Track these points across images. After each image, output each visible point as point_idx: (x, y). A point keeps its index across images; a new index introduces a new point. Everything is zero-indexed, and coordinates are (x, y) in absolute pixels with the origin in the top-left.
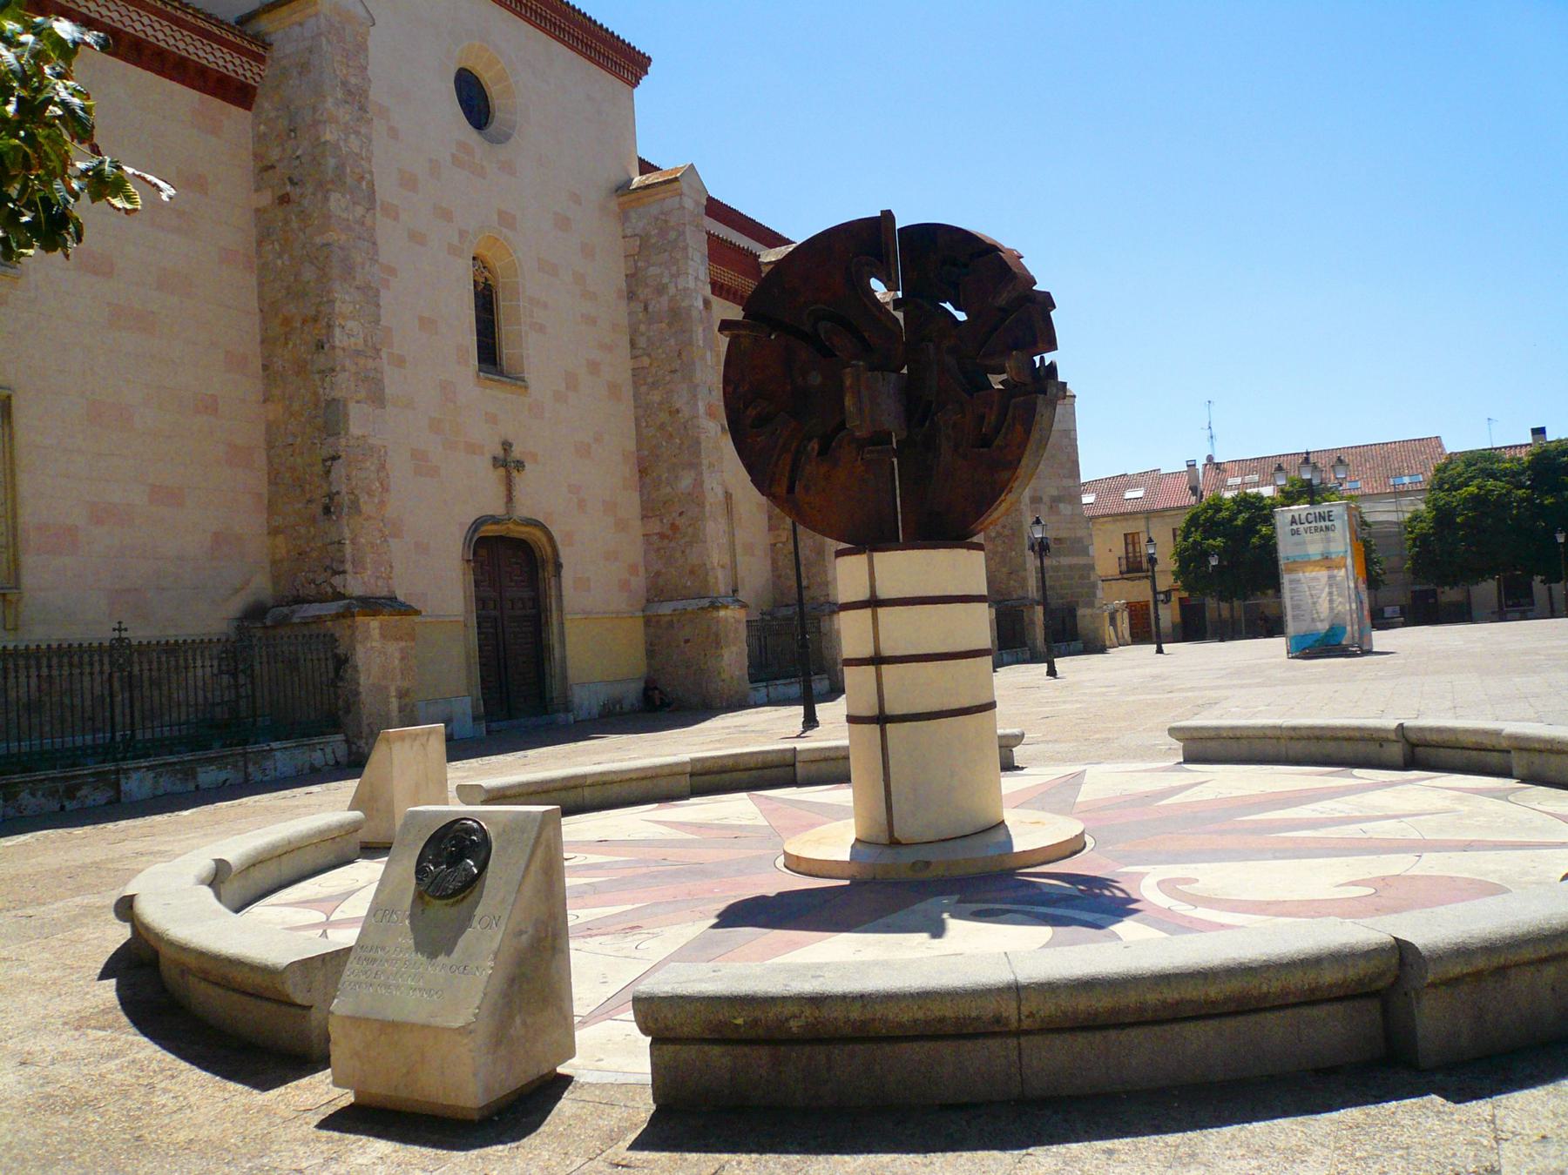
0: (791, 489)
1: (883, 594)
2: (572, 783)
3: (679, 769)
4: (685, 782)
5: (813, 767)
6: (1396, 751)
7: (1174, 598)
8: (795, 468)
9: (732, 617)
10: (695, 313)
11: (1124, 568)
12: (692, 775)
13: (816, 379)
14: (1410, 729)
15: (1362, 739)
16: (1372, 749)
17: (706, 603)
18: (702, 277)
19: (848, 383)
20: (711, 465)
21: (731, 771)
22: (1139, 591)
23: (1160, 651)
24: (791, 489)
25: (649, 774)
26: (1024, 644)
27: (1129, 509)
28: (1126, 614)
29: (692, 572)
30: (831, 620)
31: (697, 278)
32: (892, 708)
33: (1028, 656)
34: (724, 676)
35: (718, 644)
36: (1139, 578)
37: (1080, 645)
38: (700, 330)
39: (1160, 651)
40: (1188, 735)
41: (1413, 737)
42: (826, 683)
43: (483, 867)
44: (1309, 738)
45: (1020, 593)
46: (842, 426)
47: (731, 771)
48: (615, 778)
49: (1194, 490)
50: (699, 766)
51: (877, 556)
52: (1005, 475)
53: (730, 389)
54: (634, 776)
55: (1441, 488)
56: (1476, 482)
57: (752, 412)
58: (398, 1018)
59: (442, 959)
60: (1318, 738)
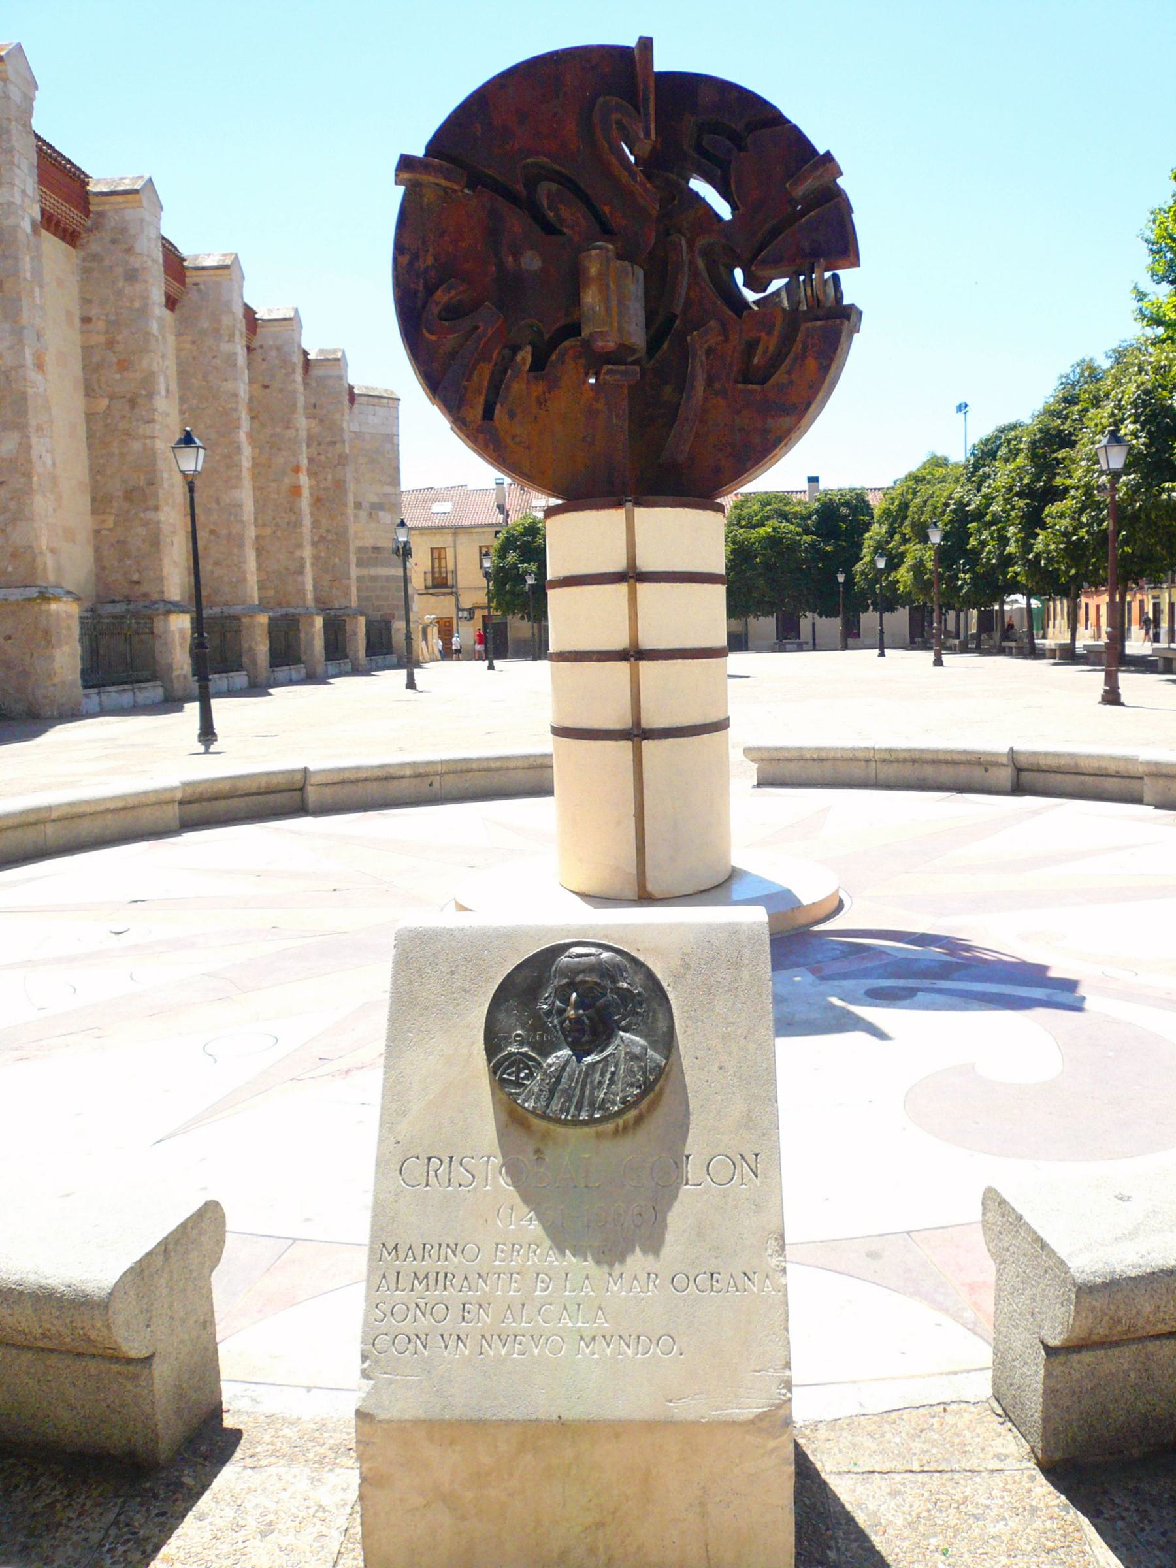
0: (488, 414)
1: (646, 564)
2: (32, 818)
3: (167, 796)
4: (172, 813)
5: (328, 791)
6: (1005, 776)
7: (479, 614)
8: (496, 388)
9: (66, 613)
10: (21, 237)
11: (429, 583)
12: (181, 803)
13: (531, 262)
14: (1017, 753)
15: (968, 763)
16: (977, 774)
17: (33, 592)
18: (30, 192)
19: (593, 271)
20: (39, 428)
21: (226, 797)
22: (444, 606)
23: (491, 667)
24: (488, 414)
25: (131, 803)
26: (346, 657)
27: (437, 522)
28: (436, 630)
29: (14, 555)
30: (166, 621)
31: (24, 192)
32: (652, 719)
33: (349, 667)
34: (56, 680)
35: (49, 644)
36: (444, 594)
37: (393, 658)
38: (28, 259)
39: (491, 667)
40: (766, 755)
41: (1023, 761)
42: (160, 691)
43: (667, 1042)
44: (905, 761)
45: (344, 603)
46: (574, 330)
47: (226, 797)
48: (87, 809)
49: (501, 508)
50: (189, 791)
51: (641, 513)
52: (786, 421)
53: (405, 260)
54: (112, 806)
55: (738, 524)
56: (771, 522)
57: (442, 297)
58: (572, 1412)
59: (637, 1261)
60: (914, 761)
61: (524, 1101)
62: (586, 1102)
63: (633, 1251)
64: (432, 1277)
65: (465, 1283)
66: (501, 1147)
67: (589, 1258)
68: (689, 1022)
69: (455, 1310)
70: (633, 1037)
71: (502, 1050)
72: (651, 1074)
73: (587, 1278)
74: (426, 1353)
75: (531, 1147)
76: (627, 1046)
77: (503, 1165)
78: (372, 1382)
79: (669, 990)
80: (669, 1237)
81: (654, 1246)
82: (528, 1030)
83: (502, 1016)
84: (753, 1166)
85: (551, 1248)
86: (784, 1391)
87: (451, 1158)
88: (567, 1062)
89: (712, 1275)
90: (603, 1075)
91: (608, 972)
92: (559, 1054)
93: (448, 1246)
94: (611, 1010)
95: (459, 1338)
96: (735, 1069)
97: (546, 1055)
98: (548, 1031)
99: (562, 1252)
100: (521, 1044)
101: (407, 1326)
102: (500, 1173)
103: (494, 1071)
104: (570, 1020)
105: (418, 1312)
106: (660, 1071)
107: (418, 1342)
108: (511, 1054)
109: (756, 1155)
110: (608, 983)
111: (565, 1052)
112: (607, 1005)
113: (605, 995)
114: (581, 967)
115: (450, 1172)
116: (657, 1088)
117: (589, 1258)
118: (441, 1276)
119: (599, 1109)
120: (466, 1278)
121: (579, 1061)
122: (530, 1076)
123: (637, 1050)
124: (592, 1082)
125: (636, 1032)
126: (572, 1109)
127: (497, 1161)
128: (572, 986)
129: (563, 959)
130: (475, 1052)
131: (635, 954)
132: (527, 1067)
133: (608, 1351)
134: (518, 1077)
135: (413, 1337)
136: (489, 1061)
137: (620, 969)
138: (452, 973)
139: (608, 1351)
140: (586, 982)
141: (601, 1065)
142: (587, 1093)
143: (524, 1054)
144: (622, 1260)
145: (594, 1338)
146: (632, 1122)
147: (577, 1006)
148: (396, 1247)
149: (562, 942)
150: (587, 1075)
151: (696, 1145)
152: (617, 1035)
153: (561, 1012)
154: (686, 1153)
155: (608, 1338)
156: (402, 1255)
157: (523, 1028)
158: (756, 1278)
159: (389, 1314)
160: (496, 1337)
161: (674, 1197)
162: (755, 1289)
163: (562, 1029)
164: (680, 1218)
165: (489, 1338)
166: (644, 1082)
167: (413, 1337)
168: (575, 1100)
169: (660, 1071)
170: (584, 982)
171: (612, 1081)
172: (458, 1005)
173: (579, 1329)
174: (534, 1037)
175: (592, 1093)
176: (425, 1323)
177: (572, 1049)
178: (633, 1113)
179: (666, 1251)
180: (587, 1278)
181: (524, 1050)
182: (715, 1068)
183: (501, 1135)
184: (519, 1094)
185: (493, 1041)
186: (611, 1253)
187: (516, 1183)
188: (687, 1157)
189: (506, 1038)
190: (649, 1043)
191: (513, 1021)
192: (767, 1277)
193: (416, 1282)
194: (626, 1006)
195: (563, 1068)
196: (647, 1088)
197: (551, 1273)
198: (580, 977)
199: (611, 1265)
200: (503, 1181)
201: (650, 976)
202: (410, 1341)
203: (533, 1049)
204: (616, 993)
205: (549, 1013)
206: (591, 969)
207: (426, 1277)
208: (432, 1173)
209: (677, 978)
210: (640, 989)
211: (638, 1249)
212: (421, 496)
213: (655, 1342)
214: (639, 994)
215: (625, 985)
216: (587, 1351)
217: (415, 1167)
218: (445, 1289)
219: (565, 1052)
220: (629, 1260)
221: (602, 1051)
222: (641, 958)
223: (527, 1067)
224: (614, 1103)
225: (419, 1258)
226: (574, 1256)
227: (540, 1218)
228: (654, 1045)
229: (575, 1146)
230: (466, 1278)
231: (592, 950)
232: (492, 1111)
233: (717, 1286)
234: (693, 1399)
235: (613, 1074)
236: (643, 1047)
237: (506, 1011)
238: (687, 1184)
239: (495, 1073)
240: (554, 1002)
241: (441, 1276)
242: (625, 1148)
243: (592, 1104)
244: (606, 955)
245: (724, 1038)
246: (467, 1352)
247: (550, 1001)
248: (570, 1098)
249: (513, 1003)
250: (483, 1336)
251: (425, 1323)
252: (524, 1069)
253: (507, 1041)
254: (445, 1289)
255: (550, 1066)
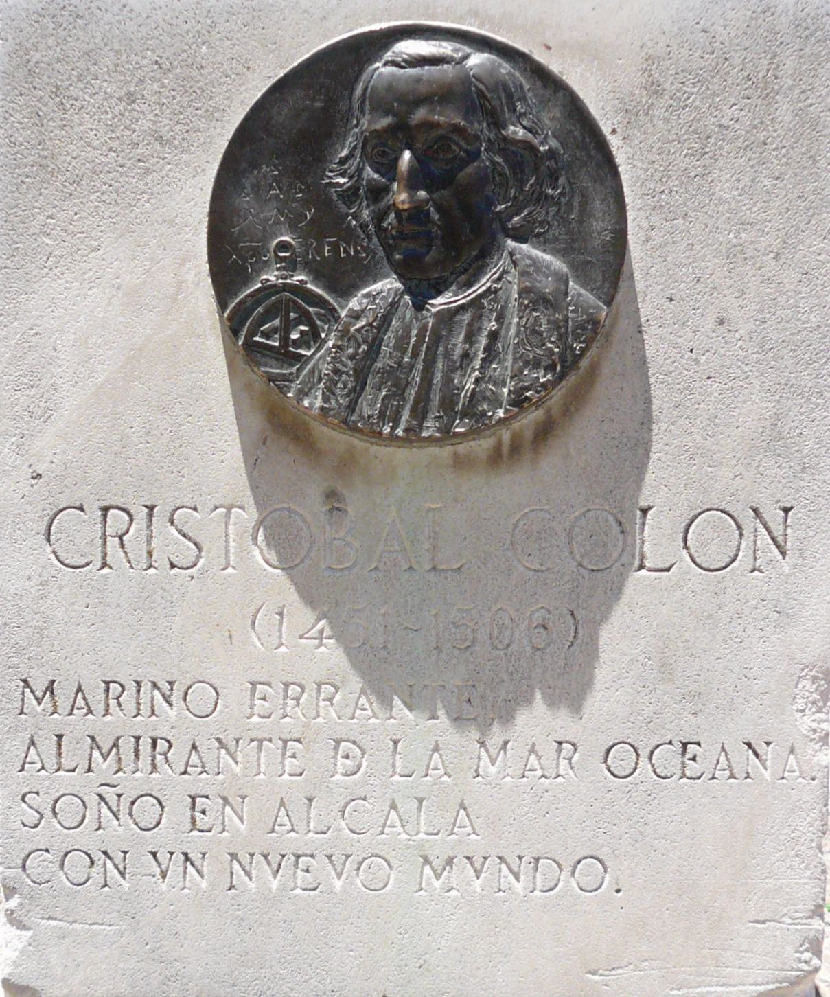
43: (609, 265)
59: (536, 721)
61: (302, 394)
62: (436, 398)
63: (529, 701)
64: (127, 746)
65: (194, 758)
66: (254, 488)
67: (441, 713)
68: (656, 219)
69: (177, 811)
70: (537, 253)
71: (247, 280)
72: (577, 338)
73: (436, 749)
74: (126, 885)
75: (314, 492)
76: (524, 274)
77: (261, 522)
78: (30, 933)
79: (614, 142)
80: (602, 674)
81: (571, 691)
82: (304, 235)
83: (245, 201)
84: (778, 532)
85: (363, 692)
86: (807, 956)
87: (151, 508)
88: (394, 306)
89: (685, 745)
90: (470, 338)
91: (482, 101)
92: (377, 286)
93: (155, 685)
94: (489, 190)
95: (187, 858)
96: (751, 326)
97: (345, 292)
98: (348, 235)
99: (386, 703)
100: (291, 265)
101: (86, 838)
102: (255, 539)
103: (234, 325)
104: (399, 213)
105: (105, 810)
106: (592, 328)
107: (109, 865)
108: (268, 289)
109: (786, 510)
110: (481, 127)
111: (389, 284)
112: (482, 179)
113: (475, 156)
114: (423, 89)
115: (150, 538)
116: (584, 363)
117: (441, 713)
118: (145, 745)
119: (464, 414)
120: (194, 747)
121: (419, 306)
122: (313, 338)
123: (547, 285)
124: (447, 354)
125: (542, 241)
126: (406, 415)
127: (247, 516)
128: (402, 133)
129: (381, 70)
130: (191, 277)
131: (540, 57)
132: (305, 318)
133: (477, 884)
134: (285, 340)
135: (98, 856)
136: (222, 305)
137: (510, 94)
138: (131, 98)
139: (477, 884)
140: (437, 125)
141: (466, 317)
142: (438, 378)
143: (299, 290)
144: (507, 718)
145: (450, 861)
146: (529, 434)
147: (412, 184)
148: (50, 688)
149: (376, 27)
150: (437, 339)
151: (664, 486)
152: (500, 249)
153: (377, 193)
154: (643, 503)
155: (478, 861)
156: (64, 706)
157: (293, 227)
158: (769, 753)
159: (48, 813)
160: (258, 858)
161: (615, 592)
162: (767, 775)
163: (380, 230)
164: (626, 635)
165: (246, 860)
166: (562, 356)
167: (98, 856)
168: (412, 393)
169: (592, 328)
170: (428, 125)
171: (491, 354)
172: (148, 171)
173: (421, 845)
174: (319, 251)
175: (447, 380)
176: (118, 832)
177: (401, 277)
178: (532, 418)
179: (595, 703)
180: (436, 749)
181: (298, 278)
182: (710, 322)
183: (253, 463)
184: (288, 379)
185: (228, 260)
186: (484, 703)
187: (288, 565)
188: (645, 511)
189: (257, 253)
190: (572, 266)
191: (271, 213)
192: (792, 751)
193: (96, 754)
194: (522, 183)
195: (385, 320)
196: (564, 365)
197: (364, 741)
198: (420, 114)
199: (485, 728)
200: (259, 555)
201: (576, 110)
202: (92, 863)
203: (317, 276)
204: (503, 152)
205: (351, 195)
206: (443, 95)
207: (115, 745)
208: (113, 542)
209: (632, 114)
210: (554, 143)
211: (538, 695)
212: (387, 249)
213: (567, 869)
214: (551, 153)
215: (521, 132)
216: (437, 884)
217: (79, 532)
218: (154, 766)
219: (389, 284)
220: (522, 718)
221: (469, 284)
222: (554, 66)
223: (305, 318)
224: (496, 402)
225: (99, 708)
226: (410, 709)
227: (340, 635)
228: (581, 270)
229: (411, 484)
230: (194, 747)
231: (445, 48)
232: (231, 409)
233: (693, 768)
234: (637, 969)
235: (494, 336)
236: (563, 280)
237: (256, 188)
238: (641, 567)
239: (235, 332)
240: (360, 171)
241: (145, 745)
242: (513, 491)
243: (448, 404)
244: (477, 59)
245: (735, 255)
246: (204, 884)
247: (353, 165)
248: (399, 390)
249: (268, 170)
250: (234, 856)
251: (118, 832)
252: (298, 322)
253: (258, 259)
254: (154, 766)
255: (356, 316)
